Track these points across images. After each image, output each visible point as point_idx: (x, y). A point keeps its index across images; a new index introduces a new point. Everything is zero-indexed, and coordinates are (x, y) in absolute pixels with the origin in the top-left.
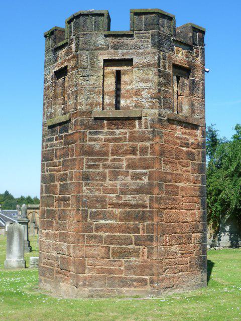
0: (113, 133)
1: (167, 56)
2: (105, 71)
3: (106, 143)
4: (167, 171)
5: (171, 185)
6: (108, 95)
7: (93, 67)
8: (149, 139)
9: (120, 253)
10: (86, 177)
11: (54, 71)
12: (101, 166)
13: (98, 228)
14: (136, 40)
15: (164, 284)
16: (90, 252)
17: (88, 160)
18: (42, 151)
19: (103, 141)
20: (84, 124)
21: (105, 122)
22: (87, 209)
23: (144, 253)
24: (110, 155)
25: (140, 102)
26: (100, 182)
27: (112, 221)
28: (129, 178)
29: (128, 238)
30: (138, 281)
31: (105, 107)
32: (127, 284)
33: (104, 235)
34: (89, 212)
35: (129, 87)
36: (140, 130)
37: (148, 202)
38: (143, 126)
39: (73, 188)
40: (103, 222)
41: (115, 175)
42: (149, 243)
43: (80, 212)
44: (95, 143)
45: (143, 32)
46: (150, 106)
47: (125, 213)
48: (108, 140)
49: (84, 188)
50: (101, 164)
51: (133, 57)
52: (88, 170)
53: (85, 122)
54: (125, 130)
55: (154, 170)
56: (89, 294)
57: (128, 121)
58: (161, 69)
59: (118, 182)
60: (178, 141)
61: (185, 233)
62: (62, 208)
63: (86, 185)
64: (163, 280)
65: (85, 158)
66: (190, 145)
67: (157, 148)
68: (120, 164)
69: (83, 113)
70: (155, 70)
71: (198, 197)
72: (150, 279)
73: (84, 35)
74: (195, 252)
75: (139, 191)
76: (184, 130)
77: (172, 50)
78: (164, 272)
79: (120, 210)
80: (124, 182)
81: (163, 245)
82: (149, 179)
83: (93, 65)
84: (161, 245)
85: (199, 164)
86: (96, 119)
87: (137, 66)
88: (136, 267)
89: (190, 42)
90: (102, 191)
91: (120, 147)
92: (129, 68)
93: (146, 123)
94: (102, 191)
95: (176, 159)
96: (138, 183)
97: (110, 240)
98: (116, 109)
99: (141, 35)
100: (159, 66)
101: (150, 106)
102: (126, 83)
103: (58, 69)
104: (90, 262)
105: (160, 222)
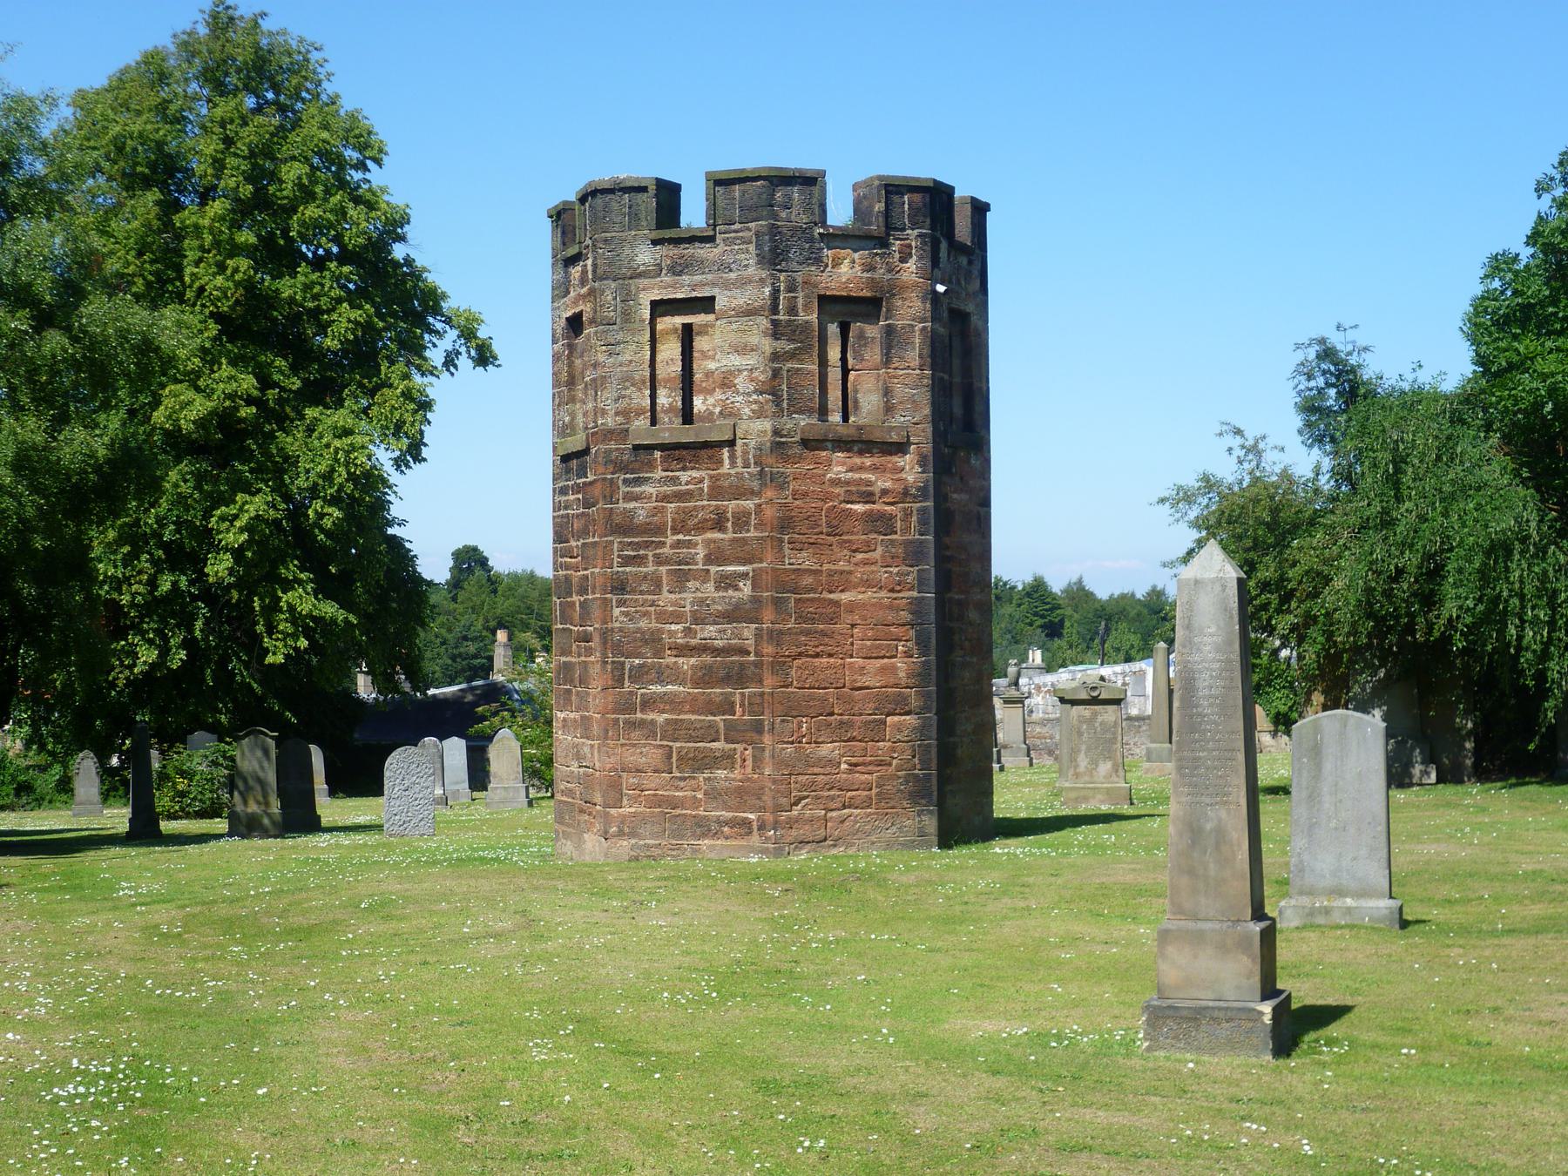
0: (675, 481)
1: (800, 280)
2: (659, 327)
3: (660, 504)
4: (802, 567)
5: (812, 600)
6: (665, 387)
7: (627, 321)
8: (753, 493)
9: (693, 759)
10: (620, 586)
12: (651, 558)
13: (648, 703)
14: (722, 247)
15: (794, 833)
16: (632, 757)
17: (623, 546)
18: (554, 517)
19: (654, 499)
20: (611, 461)
21: (658, 454)
22: (623, 659)
23: (744, 760)
24: (669, 532)
25: (732, 403)
26: (650, 597)
27: (676, 687)
28: (710, 586)
29: (712, 725)
30: (731, 823)
31: (660, 415)
32: (710, 830)
33: (661, 718)
34: (627, 666)
35: (712, 365)
36: (733, 472)
37: (751, 642)
38: (739, 461)
39: (596, 612)
40: (656, 689)
41: (681, 579)
42: (756, 737)
43: (609, 667)
44: (637, 505)
45: (737, 226)
47: (704, 667)
48: (665, 498)
49: (616, 612)
50: (651, 554)
51: (715, 292)
52: (622, 569)
54: (701, 473)
55: (764, 565)
56: (632, 853)
57: (702, 451)
58: (782, 317)
59: (689, 596)
61: (861, 714)
62: (583, 658)
63: (621, 603)
64: (790, 823)
65: (616, 540)
66: (878, 495)
68: (691, 553)
69: (608, 434)
70: (764, 322)
71: (904, 625)
72: (758, 821)
73: (606, 241)
74: (895, 762)
75: (733, 615)
76: (857, 460)
77: (818, 261)
78: (796, 804)
79: (693, 661)
80: (700, 595)
81: (792, 743)
83: (627, 316)
84: (788, 743)
85: (907, 543)
86: (637, 448)
88: (727, 792)
89: (875, 228)
90: (653, 617)
91: (689, 513)
92: (711, 317)
93: (745, 453)
94: (653, 617)
95: (829, 535)
96: (731, 598)
97: (674, 730)
98: (684, 423)
99: (733, 235)
100: (774, 309)
102: (705, 356)
104: (631, 780)
105: (782, 687)
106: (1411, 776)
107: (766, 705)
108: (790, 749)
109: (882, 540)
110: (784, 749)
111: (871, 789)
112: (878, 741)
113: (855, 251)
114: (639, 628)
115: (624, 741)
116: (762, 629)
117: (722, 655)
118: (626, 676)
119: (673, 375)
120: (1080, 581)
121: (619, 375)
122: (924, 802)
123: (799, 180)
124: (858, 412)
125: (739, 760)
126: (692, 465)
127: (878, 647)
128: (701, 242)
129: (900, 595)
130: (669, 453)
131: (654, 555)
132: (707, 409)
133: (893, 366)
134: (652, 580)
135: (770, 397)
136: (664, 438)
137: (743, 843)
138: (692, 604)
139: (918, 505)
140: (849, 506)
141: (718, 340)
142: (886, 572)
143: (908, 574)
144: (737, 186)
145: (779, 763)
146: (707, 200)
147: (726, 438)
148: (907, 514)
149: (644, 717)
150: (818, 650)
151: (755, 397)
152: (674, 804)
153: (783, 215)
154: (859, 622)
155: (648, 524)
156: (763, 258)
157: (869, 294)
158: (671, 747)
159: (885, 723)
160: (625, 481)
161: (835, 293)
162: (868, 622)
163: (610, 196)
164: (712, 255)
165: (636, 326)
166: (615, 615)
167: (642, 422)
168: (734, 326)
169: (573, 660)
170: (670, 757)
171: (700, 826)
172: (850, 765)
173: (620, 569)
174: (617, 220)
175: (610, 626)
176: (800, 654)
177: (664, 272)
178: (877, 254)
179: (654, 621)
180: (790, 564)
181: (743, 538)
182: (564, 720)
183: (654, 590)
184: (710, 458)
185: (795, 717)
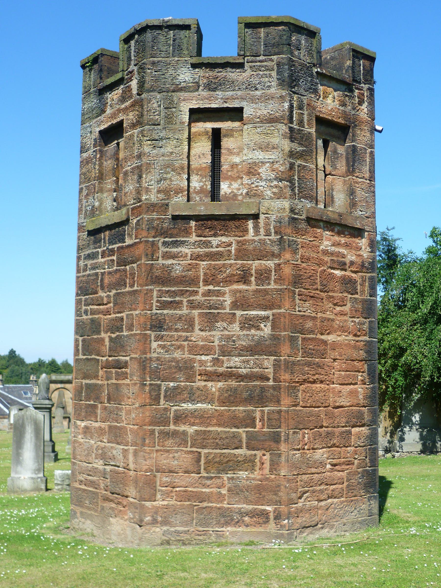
0: (207, 244)
2: (193, 130)
3: (194, 262)
6: (197, 174)
7: (170, 123)
8: (273, 255)
11: (98, 130)
12: (185, 304)
15: (299, 520)
17: (161, 294)
18: (78, 277)
19: (189, 258)
20: (153, 227)
21: (193, 223)
22: (159, 382)
24: (201, 284)
25: (257, 186)
26: (184, 334)
27: (205, 405)
28: (236, 326)
29: (235, 436)
30: (252, 514)
31: (193, 195)
32: (232, 520)
34: (163, 388)
35: (237, 160)
36: (256, 238)
37: (271, 370)
38: (262, 231)
40: (189, 406)
42: (273, 445)
43: (147, 388)
44: (174, 262)
46: (274, 193)
47: (229, 389)
48: (198, 257)
49: (154, 345)
50: (185, 300)
51: (244, 104)
53: (155, 223)
54: (229, 238)
55: (282, 311)
59: (217, 334)
60: (326, 259)
61: (338, 427)
62: (114, 381)
63: (158, 338)
65: (155, 290)
66: (348, 265)
67: (287, 271)
68: (220, 300)
69: (152, 207)
70: (283, 128)
71: (362, 361)
72: (274, 512)
73: (153, 63)
76: (337, 238)
77: (315, 91)
78: (300, 498)
79: (220, 384)
80: (227, 333)
81: (299, 450)
82: (274, 327)
83: (169, 119)
86: (175, 218)
87: (251, 121)
90: (186, 349)
91: (219, 269)
92: (237, 124)
93: (267, 224)
94: (186, 349)
95: (321, 291)
96: (253, 336)
99: (258, 64)
101: (274, 193)
102: (230, 152)
103: (106, 126)
104: (165, 479)
105: (294, 406)
106: (436, 447)
107: (283, 420)
108: (298, 454)
109: (351, 298)
110: (294, 455)
111: (343, 483)
112: (347, 447)
113: (335, 91)
114: (173, 358)
115: (159, 448)
116: (280, 360)
117: (245, 380)
118: (162, 396)
119: (204, 165)
120: (67, 361)
121: (162, 163)
122: (371, 490)
123: (305, 32)
124: (333, 205)
125: (258, 464)
126: (222, 232)
127: (348, 376)
128: (232, 68)
129: (360, 339)
130: (202, 223)
131: (188, 301)
132: (232, 192)
133: (356, 175)
134: (186, 321)
135: (288, 183)
136: (200, 211)
137: (261, 529)
138: (221, 339)
139: (369, 275)
140: (332, 271)
141: (246, 139)
142: (352, 321)
143: (364, 324)
144: (262, 29)
145: (293, 466)
146: (239, 37)
147: (253, 212)
148: (364, 281)
149: (177, 428)
150: (315, 378)
151: (275, 183)
152: (201, 498)
153: (296, 53)
154: (338, 357)
155: (184, 277)
156: (283, 81)
157: (343, 122)
158: (200, 453)
159: (350, 433)
160: (164, 243)
161: (324, 116)
162: (343, 358)
163: (158, 32)
164: (241, 77)
165: (177, 127)
166: (153, 348)
167: (181, 199)
168: (259, 130)
169: (99, 382)
170: (198, 460)
171: (224, 516)
172: (332, 465)
173: (158, 312)
174: (164, 49)
175: (148, 356)
176: (305, 381)
177: (201, 88)
178: (347, 96)
179: (186, 353)
180: (299, 311)
181: (265, 290)
182: (86, 427)
183: (187, 328)
184: (237, 227)
185: (300, 429)
